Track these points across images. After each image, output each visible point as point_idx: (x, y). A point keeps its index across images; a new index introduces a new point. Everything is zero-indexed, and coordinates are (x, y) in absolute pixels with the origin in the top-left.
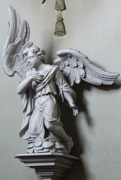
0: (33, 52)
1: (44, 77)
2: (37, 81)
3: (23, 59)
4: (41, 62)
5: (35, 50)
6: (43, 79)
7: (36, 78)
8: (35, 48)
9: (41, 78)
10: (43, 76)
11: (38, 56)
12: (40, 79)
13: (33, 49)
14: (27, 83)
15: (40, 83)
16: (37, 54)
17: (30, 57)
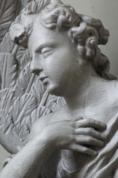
0: (53, 28)
1: (106, 133)
2: (75, 147)
3: (17, 76)
4: (91, 70)
5: (61, 17)
6: (99, 138)
7: (72, 136)
8: (60, 8)
9: (89, 134)
10: (98, 127)
11: (76, 42)
12: (87, 138)
13: (52, 13)
14: (32, 161)
15: (87, 157)
16: (69, 33)
17: (39, 51)
